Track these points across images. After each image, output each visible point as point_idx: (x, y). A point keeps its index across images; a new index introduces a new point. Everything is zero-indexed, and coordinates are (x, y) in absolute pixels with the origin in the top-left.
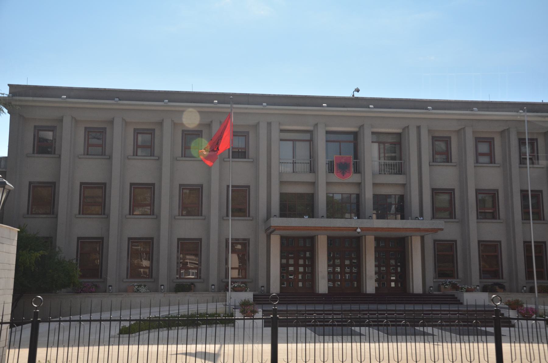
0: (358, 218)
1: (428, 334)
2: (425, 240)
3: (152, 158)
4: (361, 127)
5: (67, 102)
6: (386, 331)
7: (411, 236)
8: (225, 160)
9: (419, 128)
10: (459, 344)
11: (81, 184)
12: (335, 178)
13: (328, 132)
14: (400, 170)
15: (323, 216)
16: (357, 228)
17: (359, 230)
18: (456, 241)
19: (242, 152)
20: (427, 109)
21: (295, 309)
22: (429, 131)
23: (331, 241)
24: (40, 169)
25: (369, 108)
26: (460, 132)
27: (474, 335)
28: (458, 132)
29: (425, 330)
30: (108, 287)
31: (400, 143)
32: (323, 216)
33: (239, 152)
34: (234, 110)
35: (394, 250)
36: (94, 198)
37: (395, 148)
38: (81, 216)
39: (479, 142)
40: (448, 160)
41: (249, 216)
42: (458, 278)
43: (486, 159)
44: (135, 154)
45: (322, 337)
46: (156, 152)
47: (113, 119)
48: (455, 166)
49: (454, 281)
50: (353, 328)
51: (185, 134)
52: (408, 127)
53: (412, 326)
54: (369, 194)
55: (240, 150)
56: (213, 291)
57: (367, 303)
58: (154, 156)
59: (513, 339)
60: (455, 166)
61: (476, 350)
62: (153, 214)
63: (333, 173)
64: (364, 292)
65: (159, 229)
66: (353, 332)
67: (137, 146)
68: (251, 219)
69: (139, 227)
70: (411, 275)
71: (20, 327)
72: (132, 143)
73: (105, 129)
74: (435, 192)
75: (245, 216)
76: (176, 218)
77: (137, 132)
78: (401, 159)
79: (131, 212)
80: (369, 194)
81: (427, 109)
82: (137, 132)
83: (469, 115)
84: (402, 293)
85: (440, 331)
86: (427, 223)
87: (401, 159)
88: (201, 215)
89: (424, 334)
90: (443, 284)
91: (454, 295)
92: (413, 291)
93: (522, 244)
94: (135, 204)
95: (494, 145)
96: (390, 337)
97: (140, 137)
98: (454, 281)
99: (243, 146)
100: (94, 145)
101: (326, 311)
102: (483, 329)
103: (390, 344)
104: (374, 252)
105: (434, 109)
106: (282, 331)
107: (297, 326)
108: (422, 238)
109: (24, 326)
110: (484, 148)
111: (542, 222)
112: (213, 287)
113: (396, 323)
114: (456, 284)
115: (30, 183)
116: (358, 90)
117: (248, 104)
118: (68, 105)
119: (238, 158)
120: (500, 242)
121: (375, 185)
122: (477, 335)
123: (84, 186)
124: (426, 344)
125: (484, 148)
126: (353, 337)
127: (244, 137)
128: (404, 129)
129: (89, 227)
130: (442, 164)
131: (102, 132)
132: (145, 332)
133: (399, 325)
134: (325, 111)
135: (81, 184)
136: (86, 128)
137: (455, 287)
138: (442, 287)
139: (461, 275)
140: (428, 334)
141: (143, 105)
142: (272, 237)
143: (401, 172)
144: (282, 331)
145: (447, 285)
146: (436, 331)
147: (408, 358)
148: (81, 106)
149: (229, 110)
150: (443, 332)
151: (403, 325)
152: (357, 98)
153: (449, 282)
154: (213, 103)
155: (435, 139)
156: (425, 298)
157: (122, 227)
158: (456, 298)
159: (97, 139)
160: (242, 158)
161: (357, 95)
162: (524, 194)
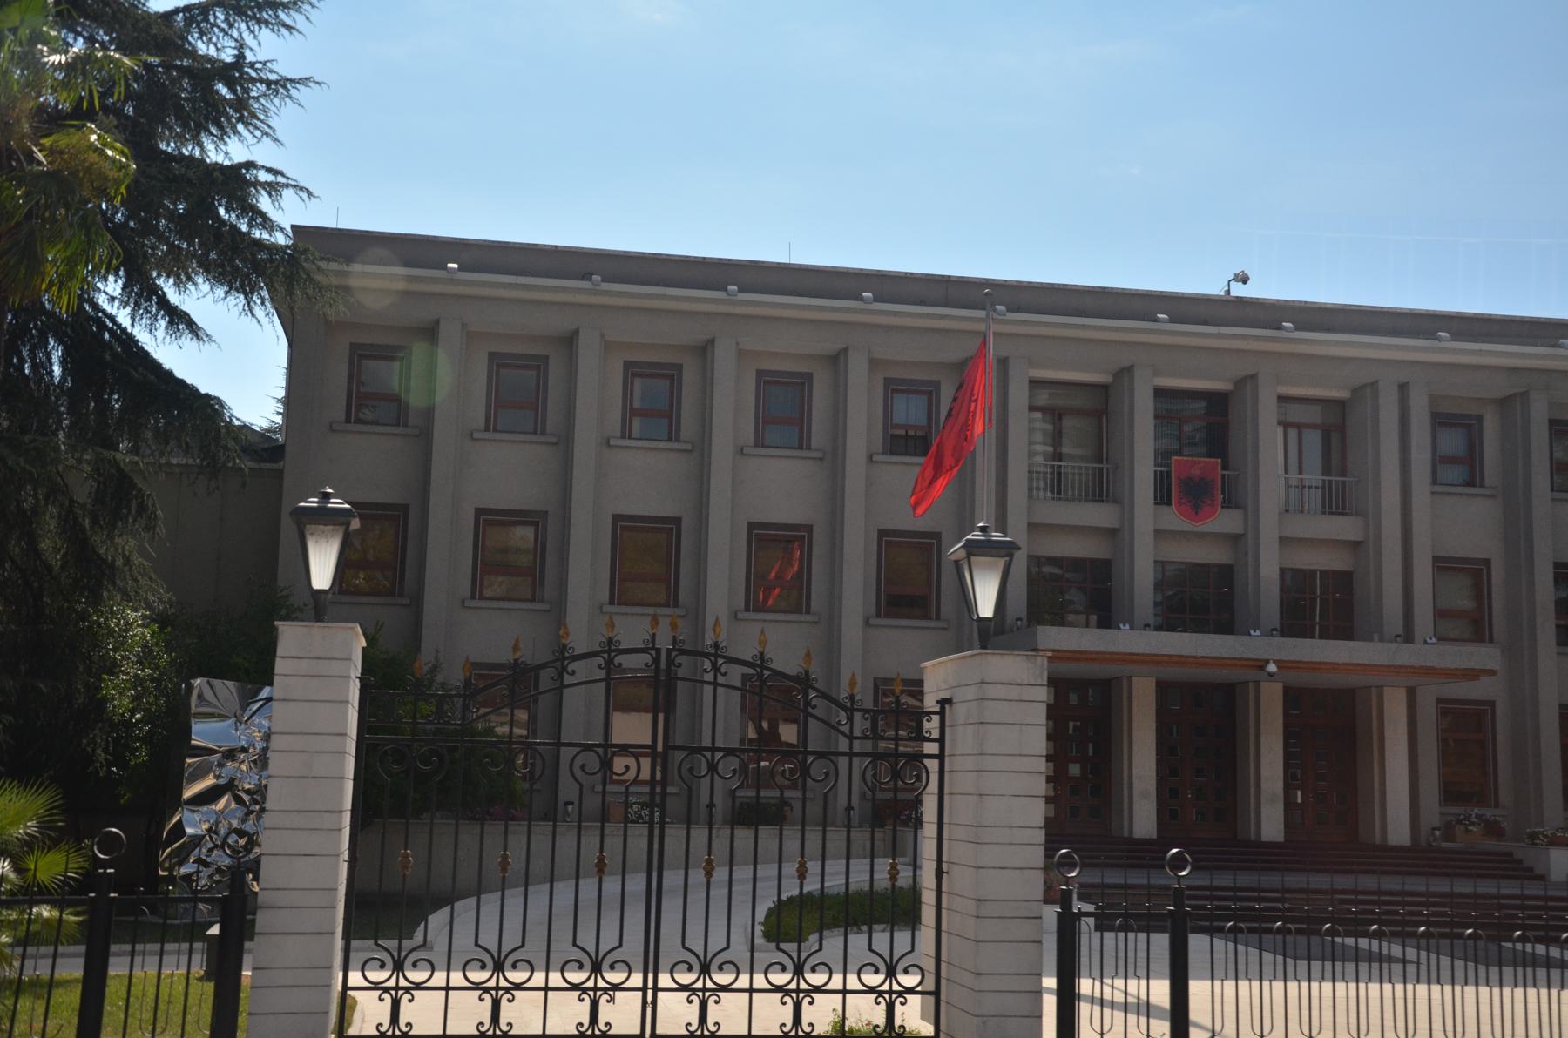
0: (1132, 628)
1: (1390, 959)
3: (400, 430)
4: (1125, 373)
5: (452, 281)
6: (1471, 952)
7: (1130, 678)
8: (476, 435)
9: (1403, 388)
10: (1377, 986)
11: (480, 512)
12: (1172, 518)
13: (1283, 399)
14: (1102, 489)
15: (1147, 626)
16: (1267, 662)
17: (1272, 668)
18: (1492, 704)
19: (915, 437)
20: (1156, 320)
21: (1097, 880)
22: (874, 364)
23: (1294, 698)
25: (861, 299)
26: (836, 360)
27: (1323, 960)
28: (1504, 403)
29: (1375, 948)
30: (560, 805)
31: (1342, 429)
32: (1147, 626)
33: (907, 437)
34: (995, 328)
35: (1330, 729)
37: (785, 408)
39: (894, 391)
40: (1473, 479)
41: (938, 618)
42: (1497, 805)
43: (1455, 473)
44: (626, 433)
45: (1303, 965)
46: (553, 418)
48: (1493, 496)
49: (1489, 813)
50: (1338, 940)
51: (766, 382)
52: (1254, 377)
53: (1490, 938)
54: (1269, 567)
55: (911, 433)
57: (1374, 872)
58: (678, 440)
59: (1219, 970)
60: (1493, 496)
61: (1327, 1003)
63: (1169, 504)
66: (1338, 952)
67: (629, 413)
70: (1377, 794)
71: (448, 908)
73: (809, 376)
74: (1442, 565)
75: (926, 617)
76: (740, 616)
78: (1343, 473)
79: (476, 592)
80: (1269, 567)
81: (861, 299)
82: (633, 371)
83: (1544, 357)
84: (1236, 849)
85: (1231, 945)
86: (1426, 653)
87: (1343, 473)
88: (808, 612)
89: (1357, 956)
90: (1459, 822)
91: (1511, 854)
92: (1131, 831)
93: (1556, 710)
94: (489, 565)
96: (1482, 969)
97: (900, 402)
98: (1489, 813)
99: (923, 421)
101: (1241, 890)
102: (1350, 941)
103: (1340, 986)
105: (878, 298)
106: (1198, 944)
107: (1126, 928)
108: (1411, 693)
109: (458, 905)
110: (1453, 442)
111: (932, 624)
113: (1309, 925)
114: (1496, 822)
116: (1244, 280)
117: (946, 304)
118: (460, 290)
119: (906, 454)
120: (1492, 704)
121: (1284, 541)
122: (1500, 965)
124: (1481, 989)
125: (1453, 442)
126: (1338, 965)
127: (925, 398)
128: (1357, 391)
130: (1459, 489)
132: (836, 931)
133: (1269, 931)
134: (452, 281)
135: (480, 512)
136: (492, 356)
137: (1493, 829)
138: (1459, 829)
139: (1505, 795)
140: (1390, 959)
141: (664, 297)
143: (1344, 507)
144: (1198, 944)
145: (1473, 824)
146: (1411, 953)
147: (1434, 1026)
148: (486, 292)
149: (982, 327)
150: (1241, 948)
151: (1279, 930)
152: (1242, 302)
153: (1477, 816)
154: (859, 298)
155: (1440, 420)
156: (1419, 857)
158: (1520, 862)
161: (1238, 290)
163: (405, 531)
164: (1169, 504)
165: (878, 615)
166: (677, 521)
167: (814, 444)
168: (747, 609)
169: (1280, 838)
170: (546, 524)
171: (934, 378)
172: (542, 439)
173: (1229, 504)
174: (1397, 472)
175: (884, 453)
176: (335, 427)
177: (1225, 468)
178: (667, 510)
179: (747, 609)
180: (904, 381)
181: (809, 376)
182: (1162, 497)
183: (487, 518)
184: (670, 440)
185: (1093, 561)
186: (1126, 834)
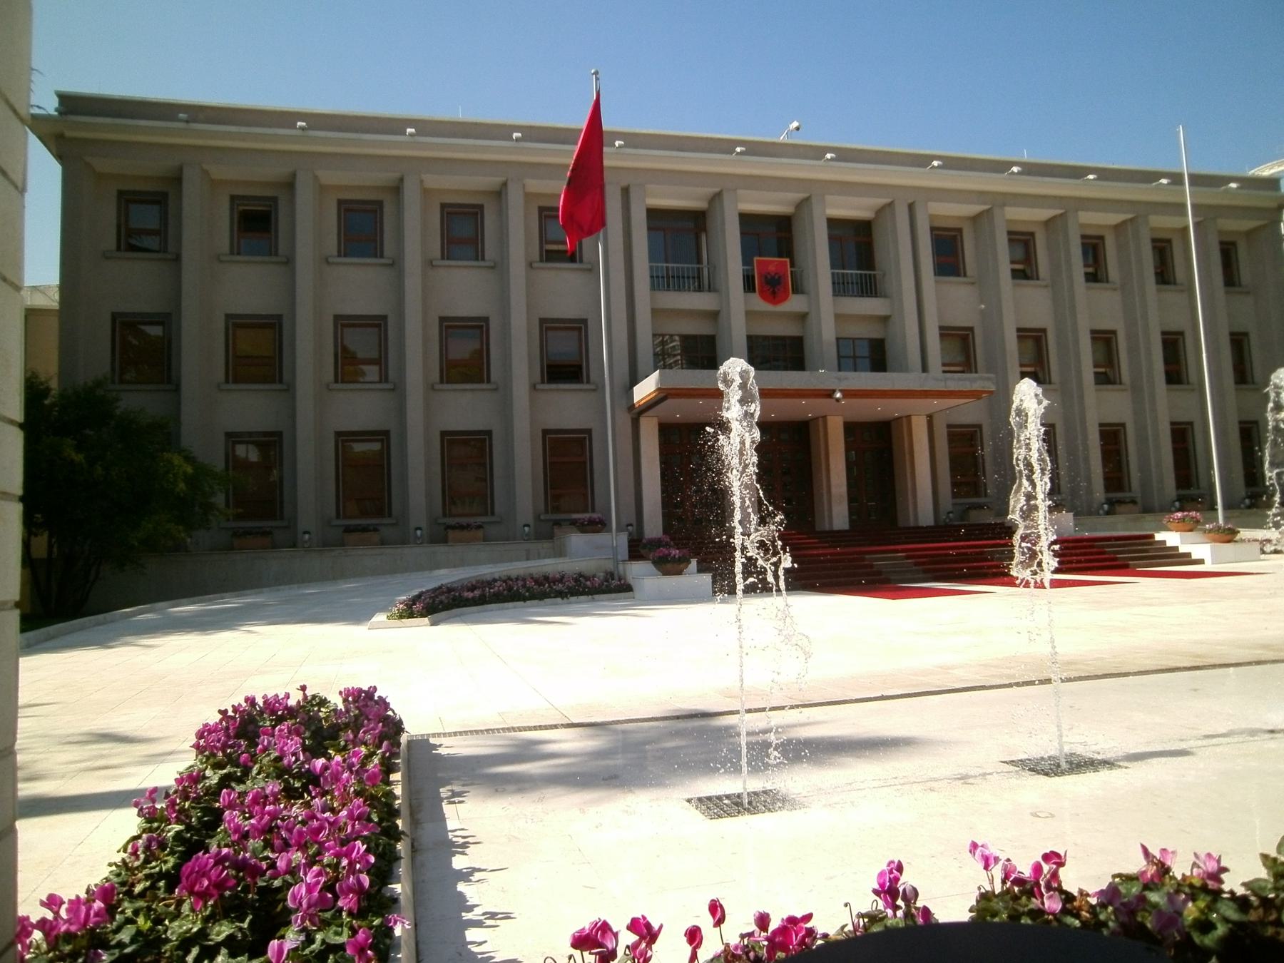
2: (935, 422)
12: (758, 302)
24: (135, 285)
26: (499, 194)
36: (259, 352)
37: (948, 251)
38: (340, 386)
41: (588, 382)
47: (294, 175)
56: (528, 538)
60: (492, 268)
62: (387, 381)
64: (827, 528)
65: (401, 411)
68: (592, 387)
69: (360, 409)
72: (335, 230)
73: (481, 207)
77: (127, 199)
82: (127, 199)
95: (382, 224)
100: (149, 233)
104: (843, 450)
111: (484, 386)
112: (419, 532)
115: (115, 316)
123: (236, 324)
129: (249, 409)
131: (473, 213)
139: (1135, 483)
142: (644, 422)
156: (940, 531)
157: (321, 412)
159: (257, 222)
160: (369, 256)
162: (1023, 334)
163: (386, 335)
164: (754, 291)
165: (543, 382)
166: (384, 318)
167: (280, 251)
168: (442, 382)
169: (846, 527)
170: (273, 327)
171: (380, 198)
172: (482, 263)
173: (797, 290)
174: (115, 236)
175: (541, 261)
176: (331, 260)
177: (792, 265)
178: (375, 310)
179: (442, 382)
180: (134, 192)
181: (481, 207)
182: (749, 285)
183: (344, 322)
184: (477, 259)
185: (701, 337)
186: (912, 524)
